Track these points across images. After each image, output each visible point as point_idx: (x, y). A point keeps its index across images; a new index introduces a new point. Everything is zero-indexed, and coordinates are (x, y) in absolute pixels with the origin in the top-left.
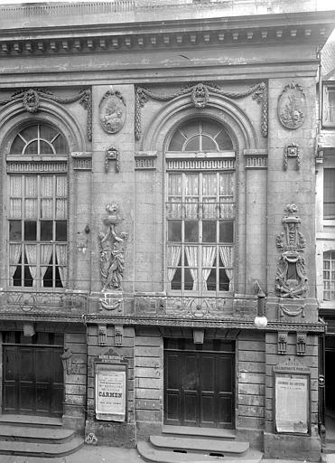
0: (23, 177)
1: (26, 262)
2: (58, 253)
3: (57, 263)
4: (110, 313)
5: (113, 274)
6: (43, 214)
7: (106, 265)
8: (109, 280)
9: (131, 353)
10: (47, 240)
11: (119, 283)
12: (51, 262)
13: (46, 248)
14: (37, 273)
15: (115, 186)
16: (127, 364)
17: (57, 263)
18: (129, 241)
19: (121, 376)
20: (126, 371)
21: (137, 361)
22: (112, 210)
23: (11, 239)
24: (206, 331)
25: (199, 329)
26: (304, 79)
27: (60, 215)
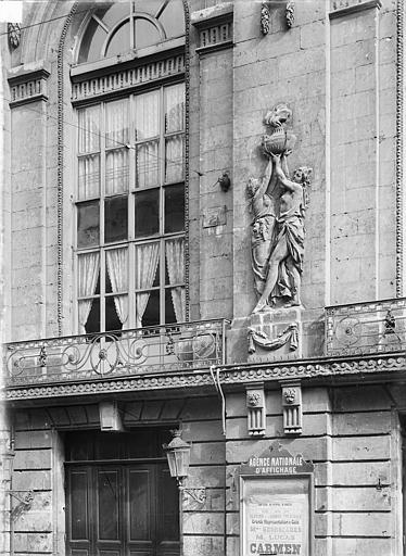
0: (131, 96)
1: (109, 289)
2: (170, 260)
3: (167, 282)
4: (271, 357)
5: (278, 267)
6: (142, 178)
7: (264, 249)
8: (271, 285)
9: (319, 450)
10: (148, 234)
11: (293, 289)
12: (156, 283)
13: (148, 252)
14: (130, 311)
15: (284, 63)
16: (307, 474)
17: (167, 282)
18: (315, 185)
19: (296, 505)
20: (309, 491)
21: (333, 474)
22: (277, 119)
23: (80, 243)
24: (123, 403)
25: (108, 399)
26: (215, 532)
27: (175, 175)
